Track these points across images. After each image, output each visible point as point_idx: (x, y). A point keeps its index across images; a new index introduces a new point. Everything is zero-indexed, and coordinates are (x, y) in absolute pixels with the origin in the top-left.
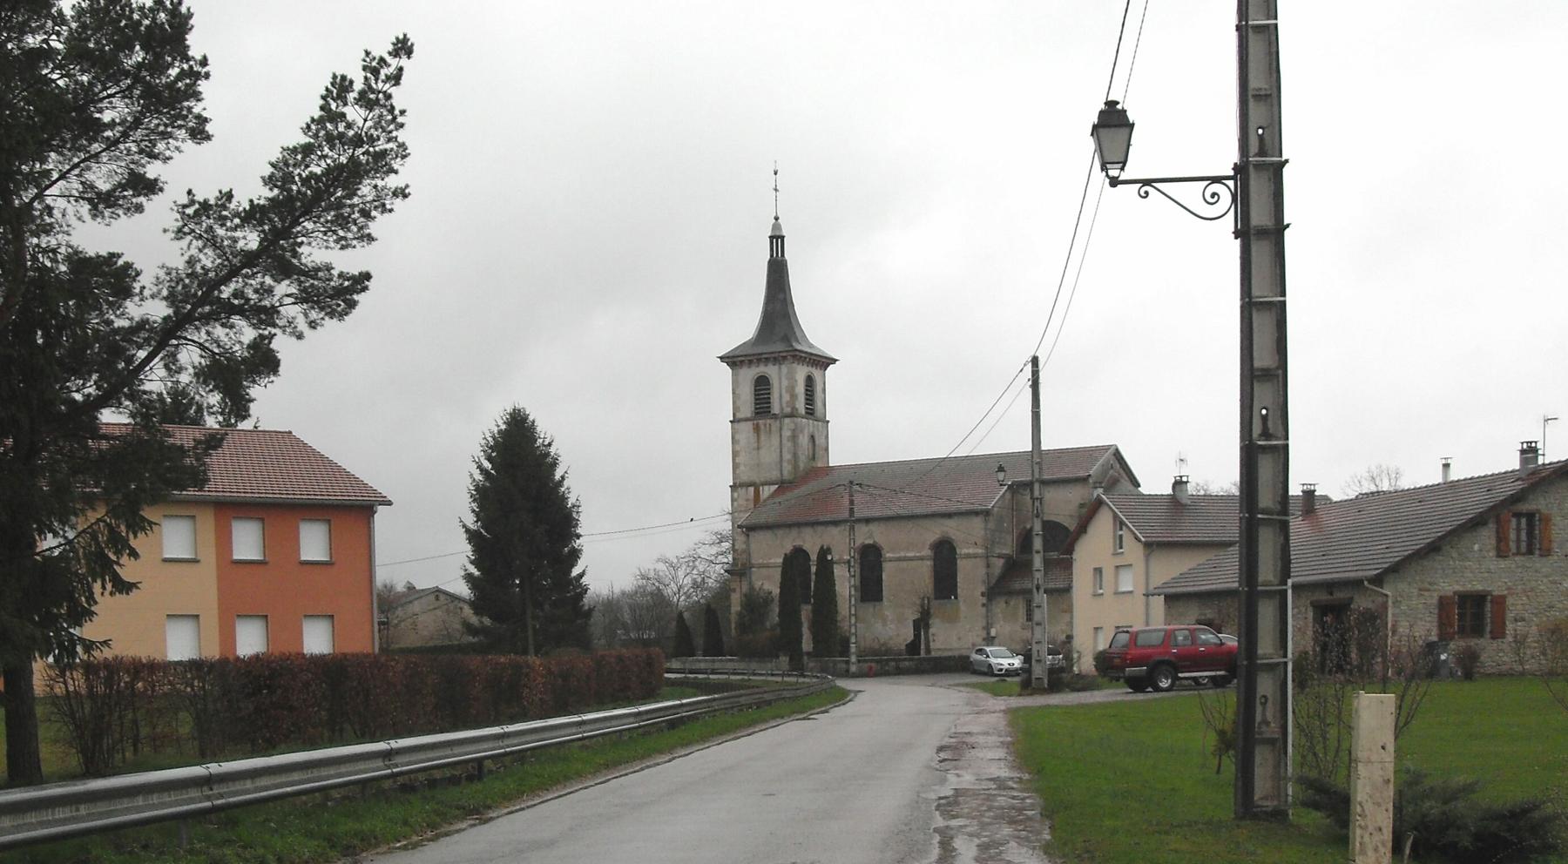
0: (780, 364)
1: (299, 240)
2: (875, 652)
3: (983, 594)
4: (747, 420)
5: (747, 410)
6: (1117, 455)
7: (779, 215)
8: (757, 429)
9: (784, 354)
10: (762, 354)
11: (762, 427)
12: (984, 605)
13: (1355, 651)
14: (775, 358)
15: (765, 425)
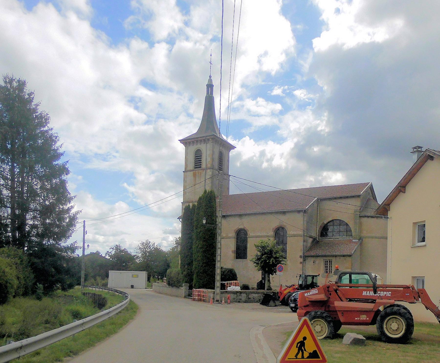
0: (207, 143)
1: (23, 95)
2: (274, 265)
3: (301, 257)
4: (191, 171)
5: (191, 166)
6: (371, 188)
7: (210, 56)
8: (195, 175)
9: (208, 138)
10: (198, 138)
11: (197, 174)
12: (301, 263)
13: (330, 320)
14: (204, 140)
15: (198, 173)
